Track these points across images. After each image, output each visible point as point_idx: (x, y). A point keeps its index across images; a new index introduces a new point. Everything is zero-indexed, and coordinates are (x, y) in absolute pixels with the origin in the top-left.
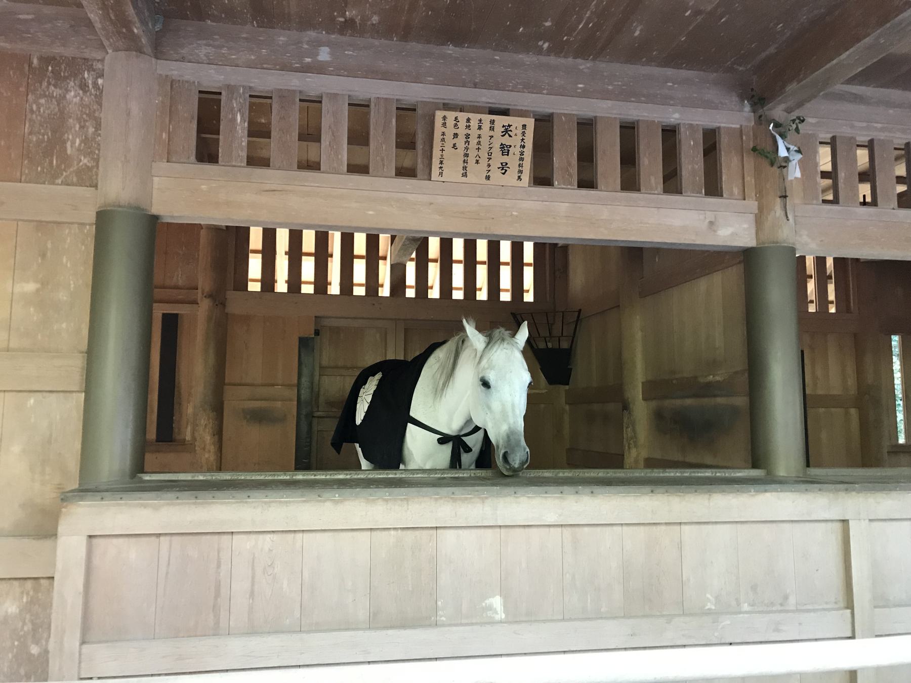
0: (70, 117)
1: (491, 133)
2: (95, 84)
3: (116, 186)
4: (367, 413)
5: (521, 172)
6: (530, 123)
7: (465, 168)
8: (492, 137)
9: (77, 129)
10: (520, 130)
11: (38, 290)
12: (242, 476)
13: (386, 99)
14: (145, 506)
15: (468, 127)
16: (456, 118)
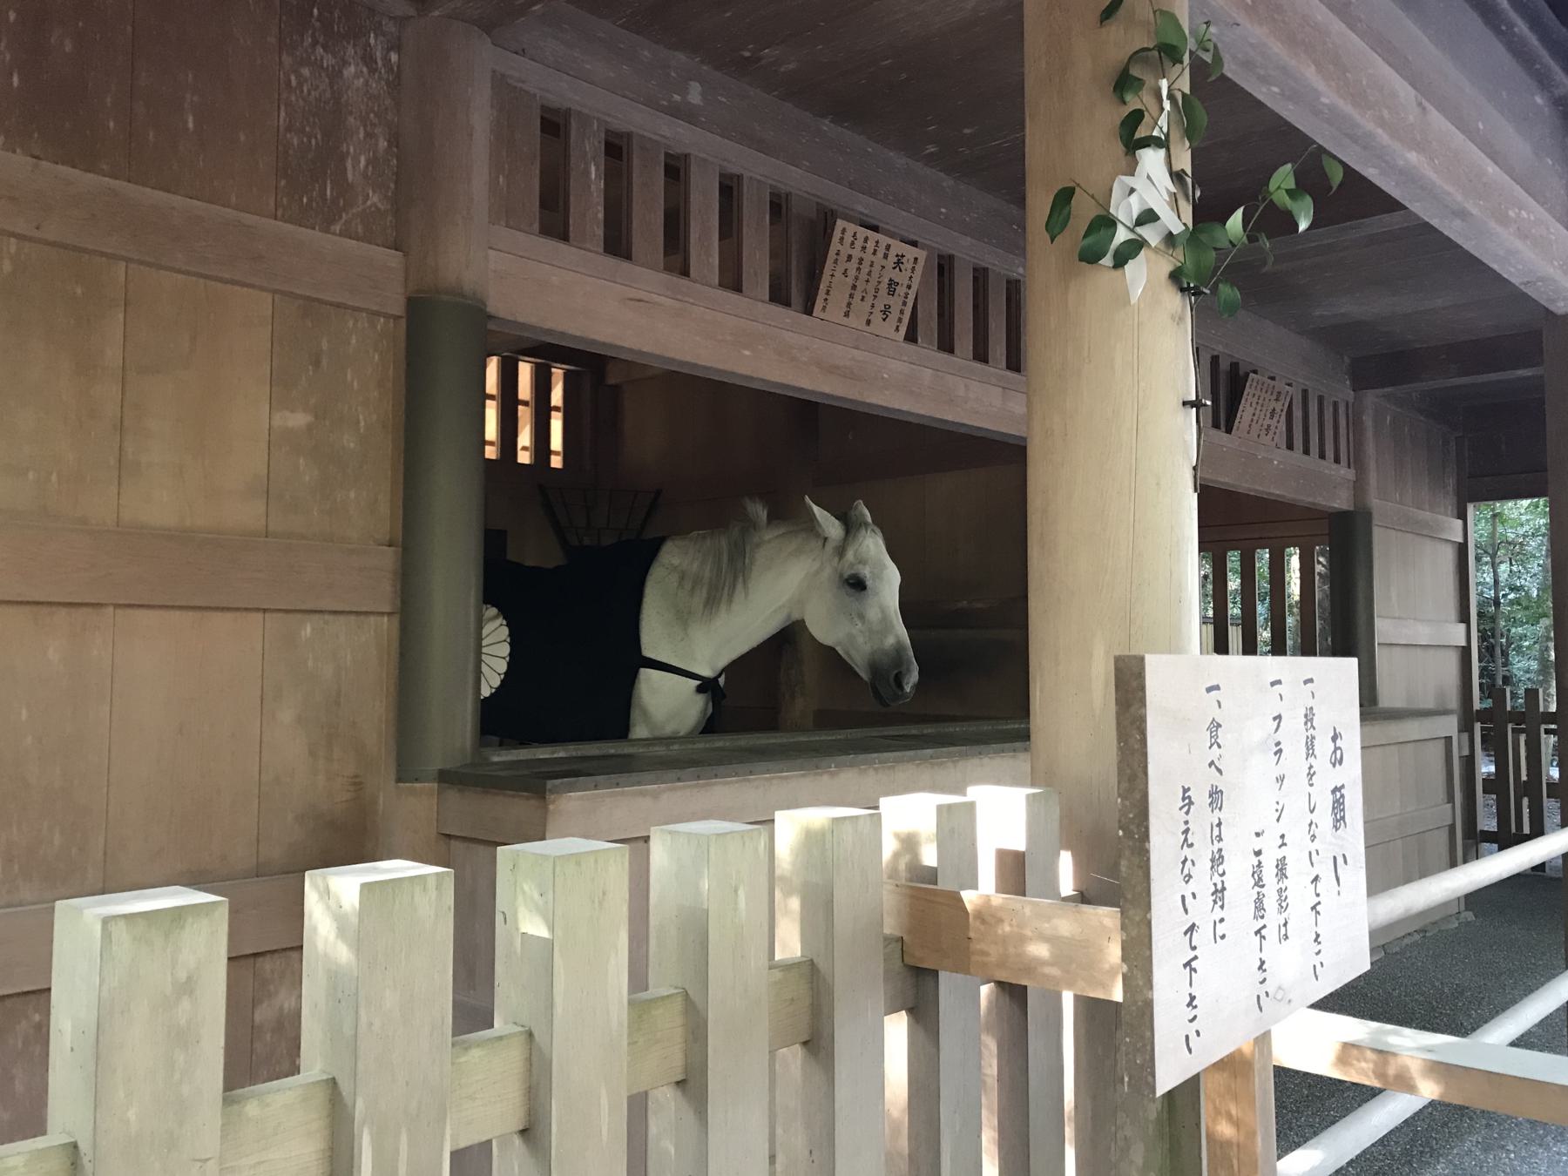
0: (351, 113)
2: (387, 60)
6: (922, 255)
7: (849, 305)
9: (362, 135)
11: (310, 427)
13: (759, 181)
14: (643, 794)
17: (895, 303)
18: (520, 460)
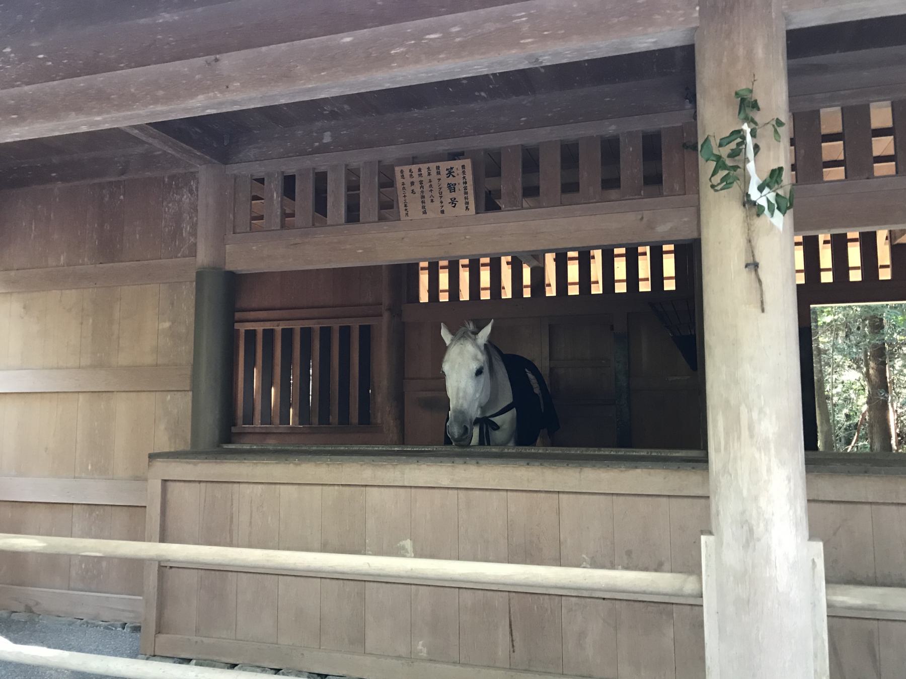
1: (439, 177)
3: (204, 257)
5: (467, 203)
6: (468, 162)
7: (423, 207)
10: (461, 170)
11: (170, 327)
12: (370, 448)
15: (420, 175)
16: (410, 170)
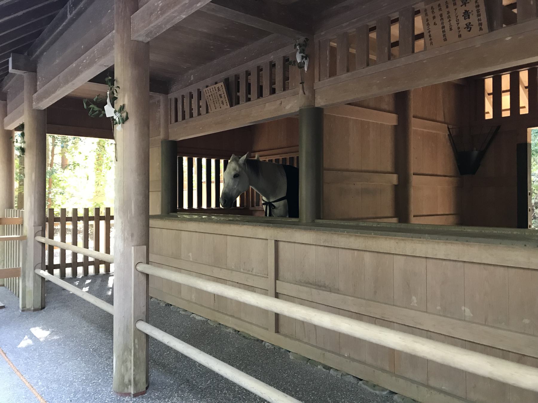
4: (192, 181)
7: (444, 35)
8: (456, 9)
17: (473, 19)
18: (509, 115)
